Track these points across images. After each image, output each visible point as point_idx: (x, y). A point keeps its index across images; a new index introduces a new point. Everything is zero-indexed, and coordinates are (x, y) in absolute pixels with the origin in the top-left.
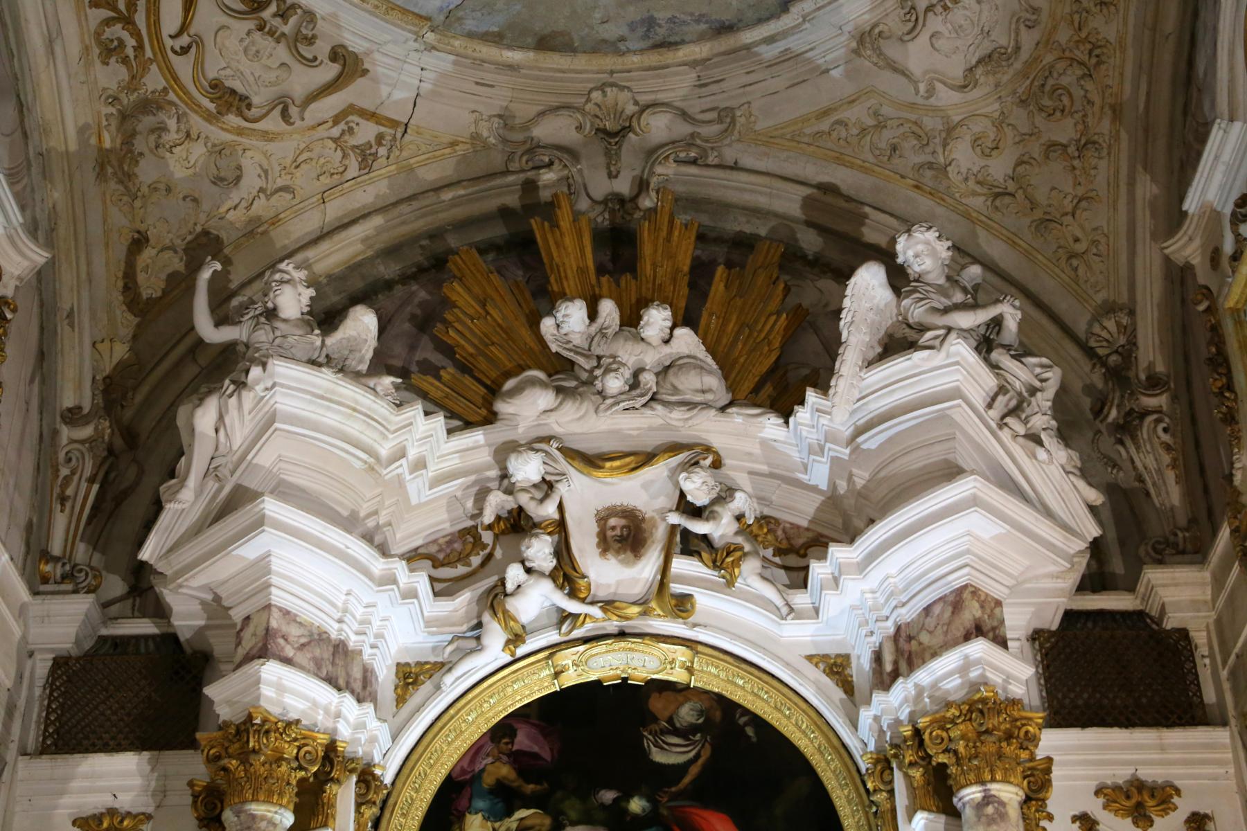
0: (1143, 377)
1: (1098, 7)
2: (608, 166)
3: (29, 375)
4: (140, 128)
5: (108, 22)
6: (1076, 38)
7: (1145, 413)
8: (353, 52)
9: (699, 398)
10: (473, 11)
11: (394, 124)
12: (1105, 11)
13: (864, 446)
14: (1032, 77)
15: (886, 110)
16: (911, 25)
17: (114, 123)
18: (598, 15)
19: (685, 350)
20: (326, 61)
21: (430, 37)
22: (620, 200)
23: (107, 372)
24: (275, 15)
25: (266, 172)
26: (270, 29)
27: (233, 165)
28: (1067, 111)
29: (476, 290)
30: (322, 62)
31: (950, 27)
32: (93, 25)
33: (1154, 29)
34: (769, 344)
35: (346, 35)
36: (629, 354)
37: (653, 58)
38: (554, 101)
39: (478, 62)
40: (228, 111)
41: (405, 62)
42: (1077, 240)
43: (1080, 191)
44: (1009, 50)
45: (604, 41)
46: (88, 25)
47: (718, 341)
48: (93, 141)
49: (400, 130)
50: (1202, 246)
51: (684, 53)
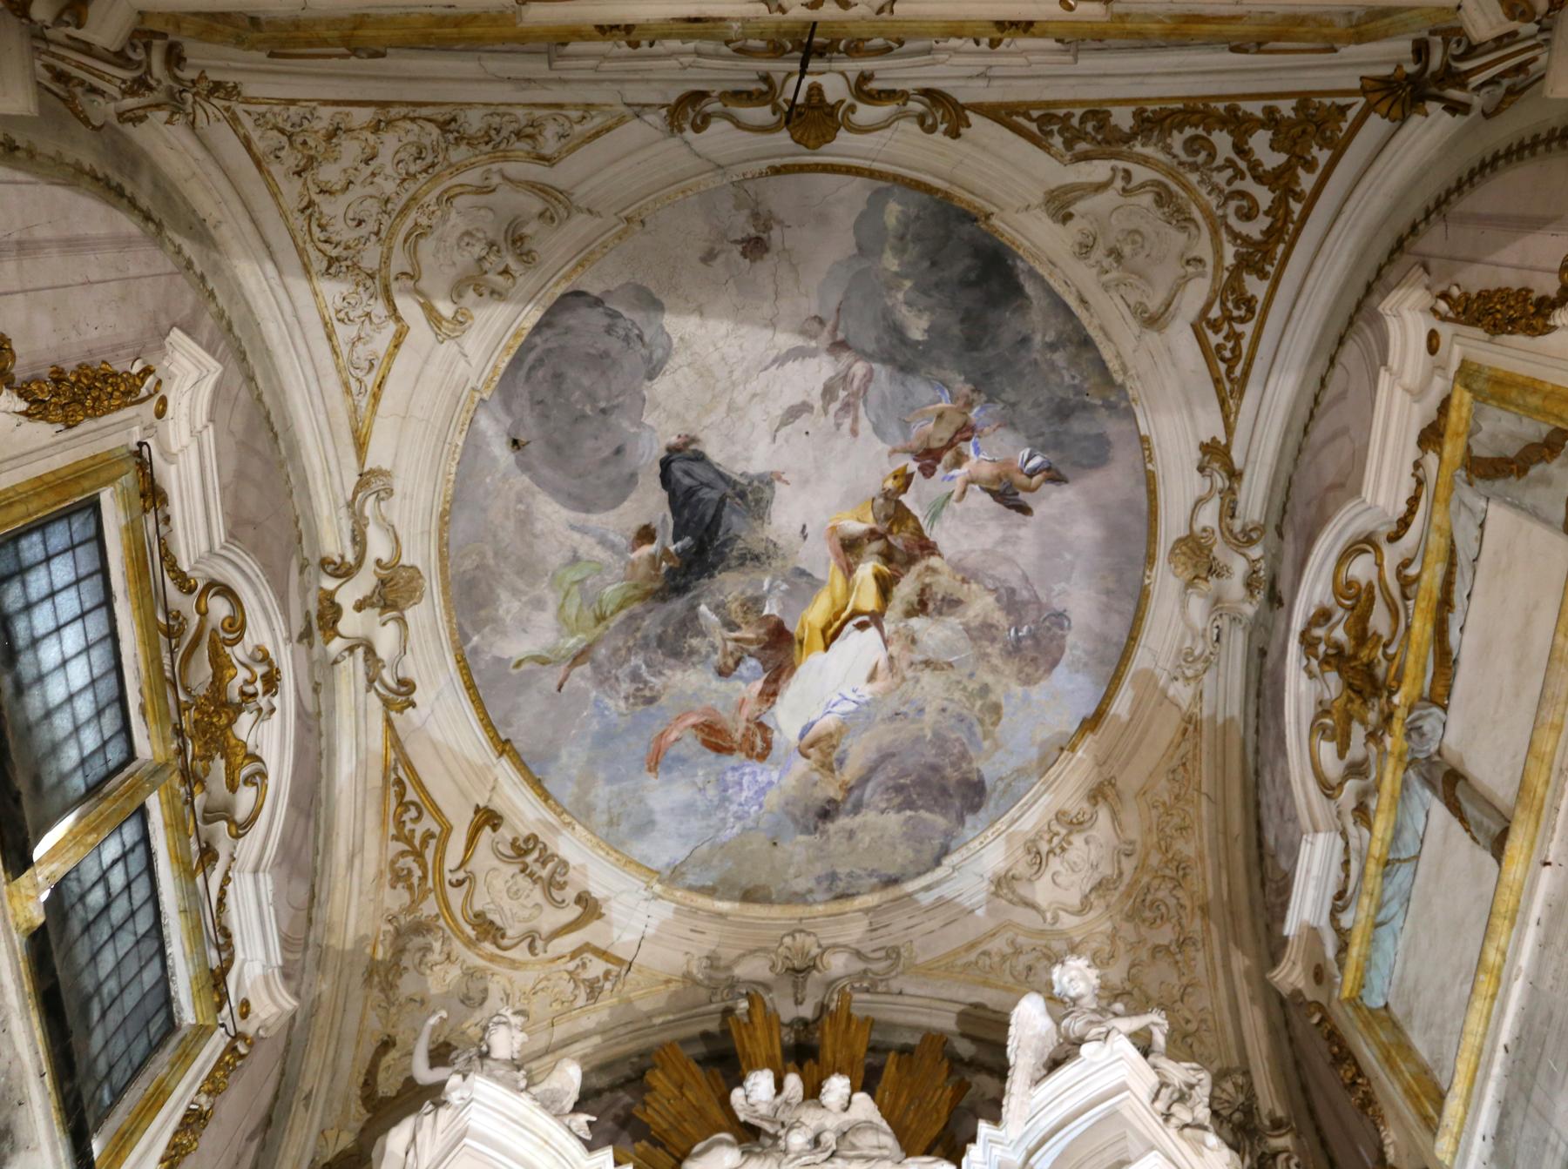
0: (1267, 1122)
2: (795, 995)
3: (249, 1131)
4: (409, 946)
5: (403, 854)
7: (1275, 1155)
9: (876, 1153)
11: (619, 961)
15: (1021, 940)
17: (389, 938)
18: (792, 871)
19: (862, 1117)
21: (658, 888)
22: (805, 1023)
23: (329, 1158)
24: (536, 860)
25: (508, 996)
27: (481, 987)
29: (675, 1076)
33: (1225, 834)
34: (938, 1112)
36: (812, 1118)
37: (835, 907)
38: (751, 945)
40: (485, 939)
42: (1188, 1021)
43: (1185, 980)
45: (796, 894)
47: (892, 1111)
48: (368, 950)
49: (625, 968)
50: (1304, 969)
51: (858, 902)
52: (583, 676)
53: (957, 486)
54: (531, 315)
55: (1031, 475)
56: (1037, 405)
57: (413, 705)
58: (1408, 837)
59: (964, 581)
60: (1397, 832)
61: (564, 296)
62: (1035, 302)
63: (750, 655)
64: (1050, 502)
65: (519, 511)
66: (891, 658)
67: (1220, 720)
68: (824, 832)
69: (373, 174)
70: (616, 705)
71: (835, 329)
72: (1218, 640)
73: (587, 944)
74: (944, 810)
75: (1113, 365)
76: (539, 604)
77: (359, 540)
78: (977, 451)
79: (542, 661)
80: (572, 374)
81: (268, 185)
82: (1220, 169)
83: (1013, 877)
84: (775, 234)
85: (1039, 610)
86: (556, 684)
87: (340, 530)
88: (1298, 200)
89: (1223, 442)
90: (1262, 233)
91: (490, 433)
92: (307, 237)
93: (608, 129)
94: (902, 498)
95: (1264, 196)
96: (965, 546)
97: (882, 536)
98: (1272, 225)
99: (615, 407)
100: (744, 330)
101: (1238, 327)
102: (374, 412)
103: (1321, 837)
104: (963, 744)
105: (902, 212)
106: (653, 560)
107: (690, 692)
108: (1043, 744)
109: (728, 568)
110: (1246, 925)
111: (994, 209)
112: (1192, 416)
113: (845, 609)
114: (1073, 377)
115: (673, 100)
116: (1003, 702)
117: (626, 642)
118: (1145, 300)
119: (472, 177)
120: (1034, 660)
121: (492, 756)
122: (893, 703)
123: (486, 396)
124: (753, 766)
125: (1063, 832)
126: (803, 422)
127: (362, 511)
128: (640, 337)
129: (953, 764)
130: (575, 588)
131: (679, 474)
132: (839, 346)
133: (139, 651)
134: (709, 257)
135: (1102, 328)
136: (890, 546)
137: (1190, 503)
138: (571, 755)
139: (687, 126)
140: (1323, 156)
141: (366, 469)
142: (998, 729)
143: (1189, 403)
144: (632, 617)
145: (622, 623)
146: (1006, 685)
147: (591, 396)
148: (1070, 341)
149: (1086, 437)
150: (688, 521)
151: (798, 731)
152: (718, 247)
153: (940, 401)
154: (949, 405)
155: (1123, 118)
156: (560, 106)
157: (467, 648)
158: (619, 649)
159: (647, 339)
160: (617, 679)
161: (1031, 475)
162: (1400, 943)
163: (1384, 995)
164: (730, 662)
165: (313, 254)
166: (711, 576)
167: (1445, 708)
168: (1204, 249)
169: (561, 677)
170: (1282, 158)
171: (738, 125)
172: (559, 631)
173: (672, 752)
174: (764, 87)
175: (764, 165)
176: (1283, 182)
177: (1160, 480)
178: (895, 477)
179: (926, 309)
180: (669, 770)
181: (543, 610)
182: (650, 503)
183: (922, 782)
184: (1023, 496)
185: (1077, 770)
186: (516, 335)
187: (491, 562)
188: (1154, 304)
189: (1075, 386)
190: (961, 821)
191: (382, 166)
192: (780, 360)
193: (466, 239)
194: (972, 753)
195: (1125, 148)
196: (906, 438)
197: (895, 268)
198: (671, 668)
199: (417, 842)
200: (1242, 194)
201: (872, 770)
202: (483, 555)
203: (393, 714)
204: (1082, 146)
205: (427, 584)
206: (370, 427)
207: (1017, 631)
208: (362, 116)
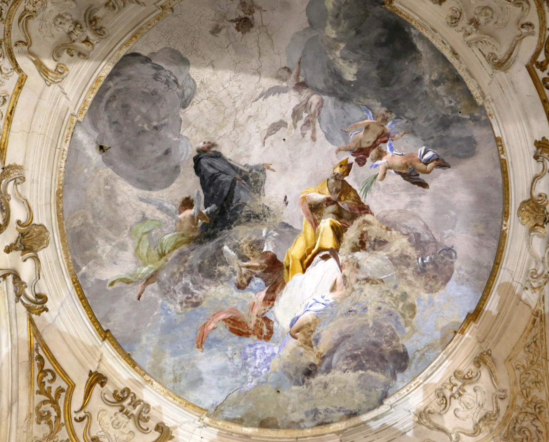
1: (534, 384)
5: (44, 402)
6: (526, 402)
8: (167, 427)
10: (229, 406)
12: (538, 385)
14: (508, 425)
16: (443, 406)
18: (290, 408)
20: (153, 431)
21: (207, 420)
24: (130, 404)
26: (126, 411)
28: (529, 439)
30: (151, 431)
31: (463, 405)
32: (36, 403)
35: (164, 417)
37: (318, 431)
39: (230, 433)
41: (193, 433)
44: (494, 412)
45: (293, 422)
46: (33, 403)
51: (334, 427)
52: (153, 290)
53: (380, 171)
55: (427, 163)
56: (428, 119)
57: (46, 310)
59: (387, 229)
61: (125, 56)
62: (424, 55)
63: (257, 276)
65: (107, 190)
66: (344, 277)
71: (298, 74)
74: (383, 370)
75: (476, 93)
76: (123, 247)
78: (392, 149)
80: (134, 105)
83: (429, 412)
84: (257, 15)
85: (436, 247)
86: (136, 295)
91: (85, 142)
94: (346, 179)
96: (387, 207)
97: (335, 202)
99: (164, 125)
100: (241, 76)
102: (9, 130)
104: (392, 329)
107: (220, 299)
108: (443, 328)
109: (240, 223)
112: (528, 124)
113: (314, 247)
114: (451, 102)
116: (416, 303)
117: (179, 269)
118: (496, 52)
120: (434, 277)
122: (347, 305)
125: (459, 384)
126: (281, 133)
128: (176, 82)
129: (387, 342)
131: (206, 166)
132: (301, 86)
134: (216, 31)
135: (468, 71)
136: (340, 208)
137: (530, 179)
138: (148, 339)
142: (414, 320)
143: (526, 116)
144: (182, 254)
145: (176, 257)
146: (418, 293)
147: (147, 118)
149: (461, 139)
150: (213, 195)
151: (289, 323)
152: (221, 25)
157: (79, 274)
159: (180, 82)
160: (175, 291)
164: (245, 280)
166: (230, 228)
169: (139, 292)
172: (137, 263)
173: (211, 336)
178: (341, 166)
180: (210, 347)
183: (368, 353)
184: (422, 176)
186: (97, 81)
187: (91, 221)
188: (501, 54)
189: (451, 107)
190: (394, 377)
192: (265, 95)
193: (59, 20)
194: (399, 335)
196: (347, 142)
197: (334, 36)
198: (208, 284)
199: (53, 395)
202: (85, 217)
203: (34, 316)
205: (51, 236)
207: (422, 260)
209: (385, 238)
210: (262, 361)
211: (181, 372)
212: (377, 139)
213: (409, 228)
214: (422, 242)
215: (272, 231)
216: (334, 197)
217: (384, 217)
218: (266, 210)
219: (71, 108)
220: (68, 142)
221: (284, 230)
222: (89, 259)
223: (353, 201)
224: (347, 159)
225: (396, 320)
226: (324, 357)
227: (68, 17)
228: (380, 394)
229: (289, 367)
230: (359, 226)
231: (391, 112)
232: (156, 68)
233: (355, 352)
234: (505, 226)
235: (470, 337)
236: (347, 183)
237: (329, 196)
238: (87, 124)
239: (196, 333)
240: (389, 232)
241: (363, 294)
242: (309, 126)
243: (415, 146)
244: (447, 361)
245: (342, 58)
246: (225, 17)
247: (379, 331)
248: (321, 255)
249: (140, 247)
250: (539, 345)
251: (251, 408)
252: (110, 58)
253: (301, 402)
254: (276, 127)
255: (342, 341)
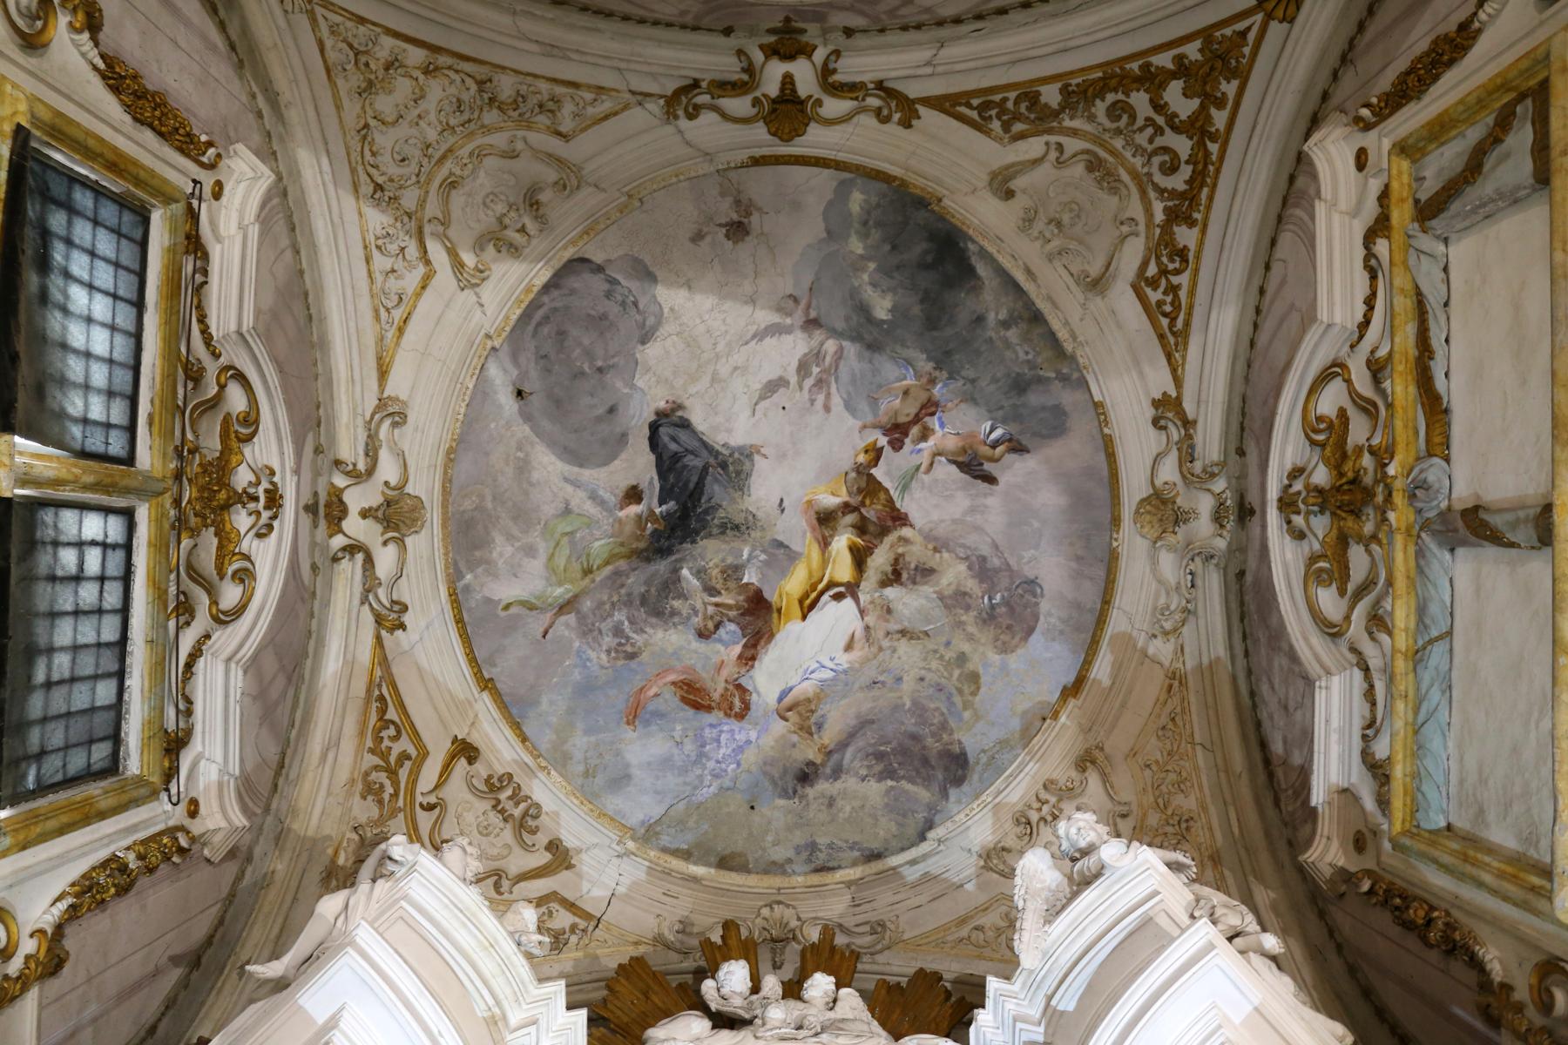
5: (376, 768)
10: (669, 827)
11: (587, 916)
13: (1060, 1008)
17: (353, 847)
18: (770, 838)
21: (631, 845)
24: (510, 798)
32: (366, 766)
37: (815, 879)
45: (774, 863)
48: (330, 851)
49: (593, 923)
50: (1341, 845)
51: (840, 875)
52: (567, 625)
53: (925, 459)
54: (541, 275)
55: (994, 446)
56: (995, 380)
57: (402, 626)
58: (1434, 609)
59: (936, 550)
60: (1421, 611)
61: (571, 261)
62: (987, 282)
63: (729, 620)
64: (1014, 471)
65: (519, 458)
66: (867, 628)
67: (1205, 661)
68: (802, 797)
69: (419, 116)
70: (598, 657)
71: (809, 306)
72: (1193, 586)
73: (555, 893)
74: (927, 781)
75: (1062, 334)
76: (530, 551)
77: (372, 452)
78: (942, 425)
79: (530, 606)
80: (574, 332)
81: (334, 95)
82: (1141, 130)
83: (1003, 849)
84: (755, 219)
85: (1011, 577)
86: (542, 629)
87: (356, 439)
88: (1214, 140)
89: (1174, 394)
90: (1186, 182)
91: (498, 382)
92: (359, 158)
93: (616, 114)
94: (873, 471)
95: (1182, 145)
96: (935, 516)
97: (856, 509)
98: (1193, 171)
99: (613, 366)
100: (728, 305)
101: (1175, 280)
102: (398, 344)
103: (1336, 680)
104: (943, 714)
105: (865, 201)
106: (640, 520)
107: (670, 650)
108: (1025, 713)
109: (710, 535)
110: (1264, 858)
111: (945, 192)
112: (1141, 374)
113: (821, 580)
114: (1027, 353)
115: (669, 93)
116: (981, 672)
117: (611, 596)
118: (1087, 267)
119: (499, 140)
120: (1009, 627)
121: (475, 690)
122: (871, 672)
123: (497, 344)
124: (731, 725)
125: (1053, 800)
126: (780, 397)
127: (377, 432)
128: (635, 304)
129: (933, 735)
130: (565, 540)
131: (666, 439)
132: (812, 324)
133: (158, 363)
134: (697, 237)
135: (1050, 298)
136: (863, 518)
137: (1149, 463)
138: (551, 703)
139: (681, 113)
140: (1229, 88)
141: (385, 395)
142: (978, 698)
143: (1137, 362)
144: (617, 573)
145: (608, 578)
146: (983, 653)
147: (589, 354)
148: (1021, 317)
149: (1044, 408)
150: (673, 486)
151: (776, 695)
152: (705, 230)
153: (905, 378)
154: (914, 382)
155: (1051, 95)
156: (575, 85)
157: (460, 584)
158: (604, 603)
159: (641, 306)
160: (600, 631)
161: (994, 446)
162: (1450, 744)
163: (1445, 813)
164: (711, 625)
165: (363, 177)
166: (694, 542)
167: (1447, 460)
168: (1135, 209)
169: (546, 625)
170: (1195, 103)
171: (724, 116)
172: (547, 579)
173: (651, 707)
174: (745, 77)
175: (743, 155)
176: (1197, 127)
177: (1117, 441)
178: (866, 452)
179: (889, 289)
180: (647, 723)
181: (534, 557)
182: (638, 465)
183: (903, 751)
184: (987, 466)
185: (1062, 739)
186: (528, 290)
187: (490, 505)
188: (1095, 269)
189: (1028, 361)
190: (945, 795)
191: (427, 112)
192: (760, 335)
193: (491, 197)
194: (952, 723)
195: (1055, 124)
196: (875, 414)
197: (860, 251)
198: (652, 626)
199: (392, 759)
200: (1165, 150)
201: (851, 736)
202: (482, 497)
203: (384, 633)
204: (1018, 127)
205: (428, 515)
206: (393, 357)
207: (990, 599)
208: (416, 55)
209: (931, 564)
210: (729, 750)
211: (598, 761)
212: (921, 409)
213: (969, 548)
214: (989, 570)
215: (758, 552)
216: (854, 501)
217: (931, 530)
218: (751, 518)
219: (487, 326)
220: (475, 377)
221: (777, 552)
222: (480, 562)
223: (884, 506)
224: (875, 442)
225: (949, 698)
226: (830, 752)
227: (503, 197)
228: (921, 824)
229: (771, 765)
230: (892, 546)
231: (941, 369)
232: (610, 282)
233: (882, 748)
234: (1116, 540)
235: (1068, 723)
236: (875, 478)
237: (846, 498)
238: (504, 354)
239: (628, 700)
240: (938, 555)
241: (896, 655)
242: (821, 388)
243: (977, 421)
244: (1031, 764)
245: (871, 284)
246: (712, 219)
247: (920, 716)
248: (831, 592)
249: (557, 554)
250: (1180, 723)
251: (706, 832)
252: (550, 260)
253: (789, 829)
254: (773, 386)
255: (861, 728)
